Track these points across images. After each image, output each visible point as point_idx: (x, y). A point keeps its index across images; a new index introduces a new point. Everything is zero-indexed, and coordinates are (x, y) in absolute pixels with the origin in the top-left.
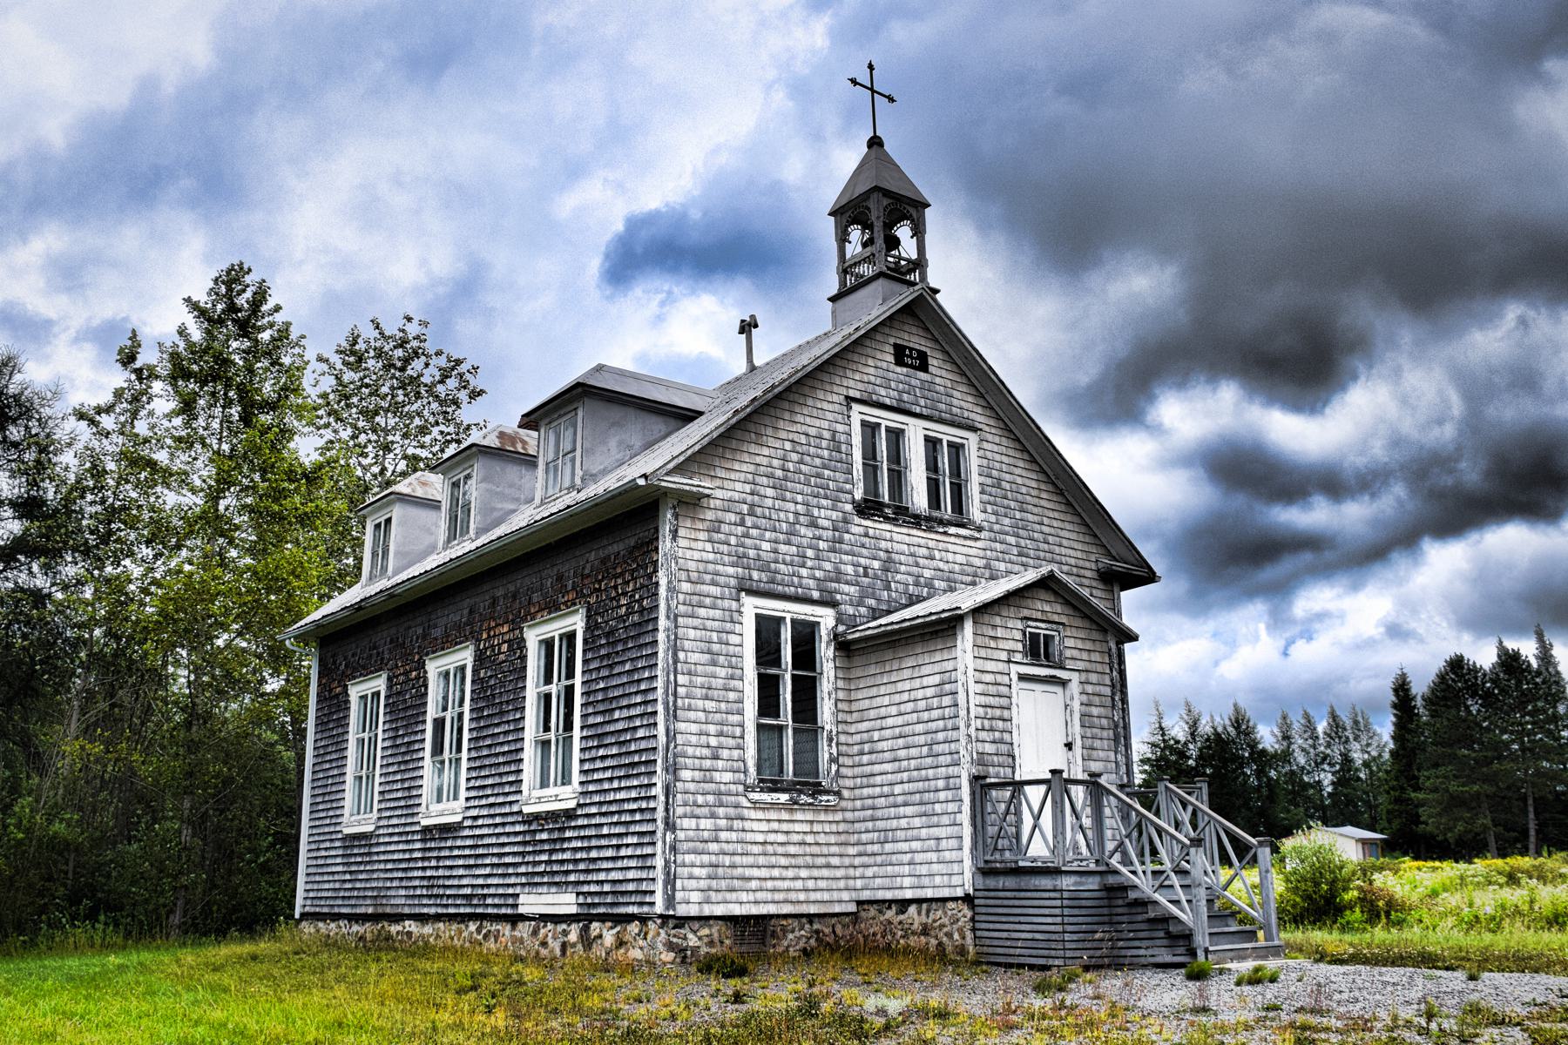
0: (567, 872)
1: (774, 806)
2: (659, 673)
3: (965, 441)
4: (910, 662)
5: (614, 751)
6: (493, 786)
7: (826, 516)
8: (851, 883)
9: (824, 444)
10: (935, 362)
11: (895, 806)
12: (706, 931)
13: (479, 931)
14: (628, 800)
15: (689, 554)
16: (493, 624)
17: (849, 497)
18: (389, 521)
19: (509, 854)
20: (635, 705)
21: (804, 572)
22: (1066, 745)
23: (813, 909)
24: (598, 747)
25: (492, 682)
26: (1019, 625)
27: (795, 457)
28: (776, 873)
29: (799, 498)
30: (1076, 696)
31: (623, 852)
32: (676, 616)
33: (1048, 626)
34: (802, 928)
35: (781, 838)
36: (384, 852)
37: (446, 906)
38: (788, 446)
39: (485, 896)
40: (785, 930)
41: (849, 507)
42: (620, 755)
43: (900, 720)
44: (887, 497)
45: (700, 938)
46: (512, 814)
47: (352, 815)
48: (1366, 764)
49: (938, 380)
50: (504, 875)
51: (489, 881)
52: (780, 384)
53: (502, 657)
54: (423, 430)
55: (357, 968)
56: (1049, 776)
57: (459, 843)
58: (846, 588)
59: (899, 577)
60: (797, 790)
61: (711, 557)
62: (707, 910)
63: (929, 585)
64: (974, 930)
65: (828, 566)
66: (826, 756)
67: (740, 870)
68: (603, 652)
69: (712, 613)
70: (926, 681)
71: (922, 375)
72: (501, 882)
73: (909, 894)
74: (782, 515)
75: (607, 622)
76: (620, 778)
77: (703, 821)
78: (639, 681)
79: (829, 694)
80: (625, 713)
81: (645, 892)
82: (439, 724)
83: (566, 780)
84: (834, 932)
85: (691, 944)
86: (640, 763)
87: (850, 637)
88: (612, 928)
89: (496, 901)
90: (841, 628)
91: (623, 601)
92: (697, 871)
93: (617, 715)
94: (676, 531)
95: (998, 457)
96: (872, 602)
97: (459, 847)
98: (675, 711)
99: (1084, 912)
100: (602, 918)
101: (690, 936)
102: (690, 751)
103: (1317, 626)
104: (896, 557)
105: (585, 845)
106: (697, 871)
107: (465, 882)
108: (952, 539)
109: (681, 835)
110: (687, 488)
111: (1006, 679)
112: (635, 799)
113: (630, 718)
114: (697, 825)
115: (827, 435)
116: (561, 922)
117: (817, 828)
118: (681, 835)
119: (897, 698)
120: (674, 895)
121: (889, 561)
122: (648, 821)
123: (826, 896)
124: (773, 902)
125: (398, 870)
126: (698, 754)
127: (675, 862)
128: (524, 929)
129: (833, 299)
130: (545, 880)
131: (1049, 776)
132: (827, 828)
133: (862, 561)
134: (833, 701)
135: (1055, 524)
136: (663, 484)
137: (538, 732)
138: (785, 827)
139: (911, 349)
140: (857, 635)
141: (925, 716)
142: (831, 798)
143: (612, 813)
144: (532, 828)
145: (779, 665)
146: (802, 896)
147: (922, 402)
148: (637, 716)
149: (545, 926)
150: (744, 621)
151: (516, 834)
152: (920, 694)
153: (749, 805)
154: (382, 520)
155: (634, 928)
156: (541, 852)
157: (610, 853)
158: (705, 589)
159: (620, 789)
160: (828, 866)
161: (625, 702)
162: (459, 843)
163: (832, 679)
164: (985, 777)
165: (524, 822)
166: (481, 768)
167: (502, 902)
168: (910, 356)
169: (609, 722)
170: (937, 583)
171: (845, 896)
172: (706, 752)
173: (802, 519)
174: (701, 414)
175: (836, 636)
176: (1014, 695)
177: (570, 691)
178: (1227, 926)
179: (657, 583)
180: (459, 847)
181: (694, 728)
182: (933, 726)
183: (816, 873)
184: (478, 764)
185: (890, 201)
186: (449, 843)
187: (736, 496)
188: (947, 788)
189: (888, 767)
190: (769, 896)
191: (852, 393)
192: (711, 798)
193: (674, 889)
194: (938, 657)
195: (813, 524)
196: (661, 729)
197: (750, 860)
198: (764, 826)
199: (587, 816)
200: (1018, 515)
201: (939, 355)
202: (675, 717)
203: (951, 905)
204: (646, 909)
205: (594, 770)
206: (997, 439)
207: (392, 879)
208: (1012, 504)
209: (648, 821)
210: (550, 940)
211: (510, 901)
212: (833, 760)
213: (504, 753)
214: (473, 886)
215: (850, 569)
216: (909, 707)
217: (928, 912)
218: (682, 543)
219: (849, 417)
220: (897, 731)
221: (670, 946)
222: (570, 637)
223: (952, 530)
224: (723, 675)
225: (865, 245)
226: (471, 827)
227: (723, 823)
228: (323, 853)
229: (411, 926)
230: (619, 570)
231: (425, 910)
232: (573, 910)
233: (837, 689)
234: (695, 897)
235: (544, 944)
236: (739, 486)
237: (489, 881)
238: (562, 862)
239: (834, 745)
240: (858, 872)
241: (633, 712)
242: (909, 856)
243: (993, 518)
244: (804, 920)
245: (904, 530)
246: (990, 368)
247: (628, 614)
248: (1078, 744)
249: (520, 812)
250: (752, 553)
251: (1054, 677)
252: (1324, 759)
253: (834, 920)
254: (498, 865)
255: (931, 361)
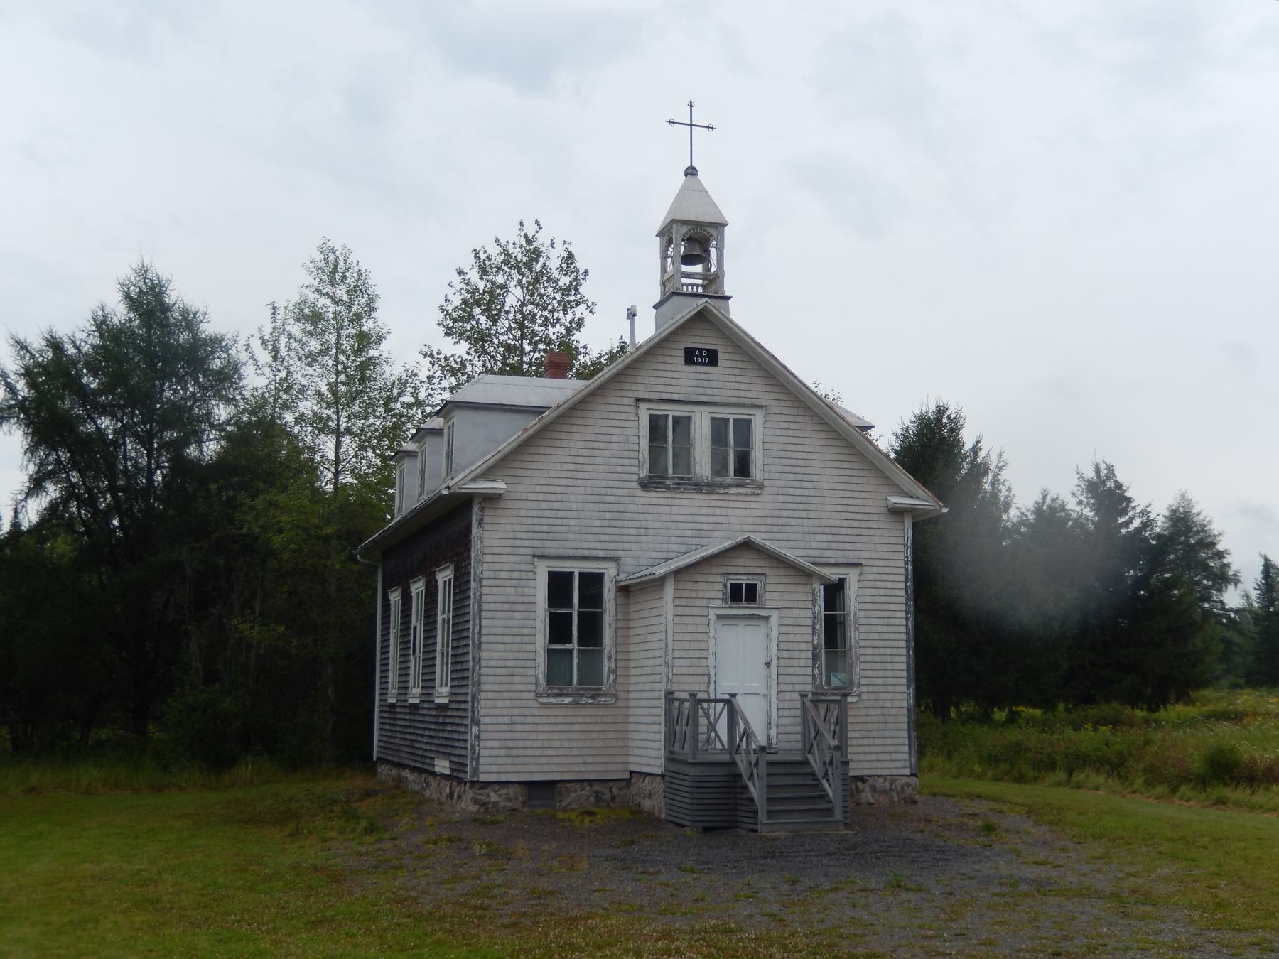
10: (726, 356)
22: (766, 664)
23: (593, 777)
26: (721, 579)
33: (749, 577)
34: (584, 789)
40: (568, 791)
44: (670, 471)
45: (500, 796)
52: (565, 403)
79: (610, 624)
84: (611, 792)
85: (492, 799)
94: (482, 519)
99: (711, 790)
101: (492, 794)
108: (733, 498)
111: (705, 620)
118: (483, 728)
127: (479, 745)
129: (656, 307)
134: (613, 629)
139: (701, 350)
142: (609, 699)
167: (419, 759)
168: (701, 356)
178: (816, 804)
185: (689, 227)
201: (730, 349)
212: (610, 672)
218: (487, 527)
219: (637, 414)
221: (475, 801)
223: (733, 490)
232: (448, 772)
233: (616, 620)
239: (612, 660)
244: (586, 784)
246: (772, 356)
248: (774, 662)
253: (611, 784)
255: (720, 356)
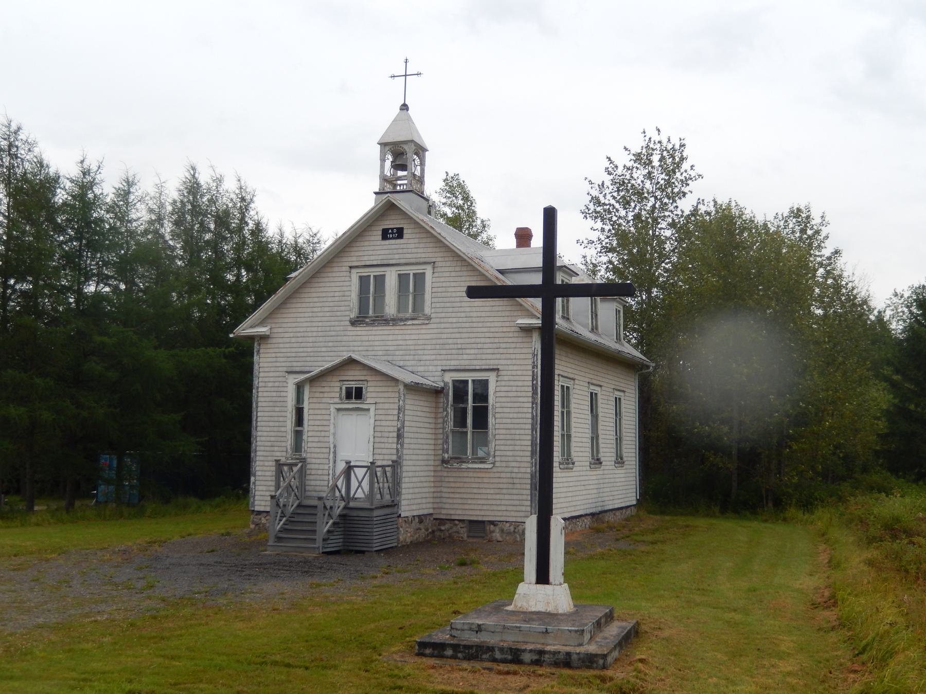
3: (385, 273)
33: (356, 383)
45: (267, 520)
55: (507, 557)
56: (370, 464)
101: (263, 519)
136: (242, 334)
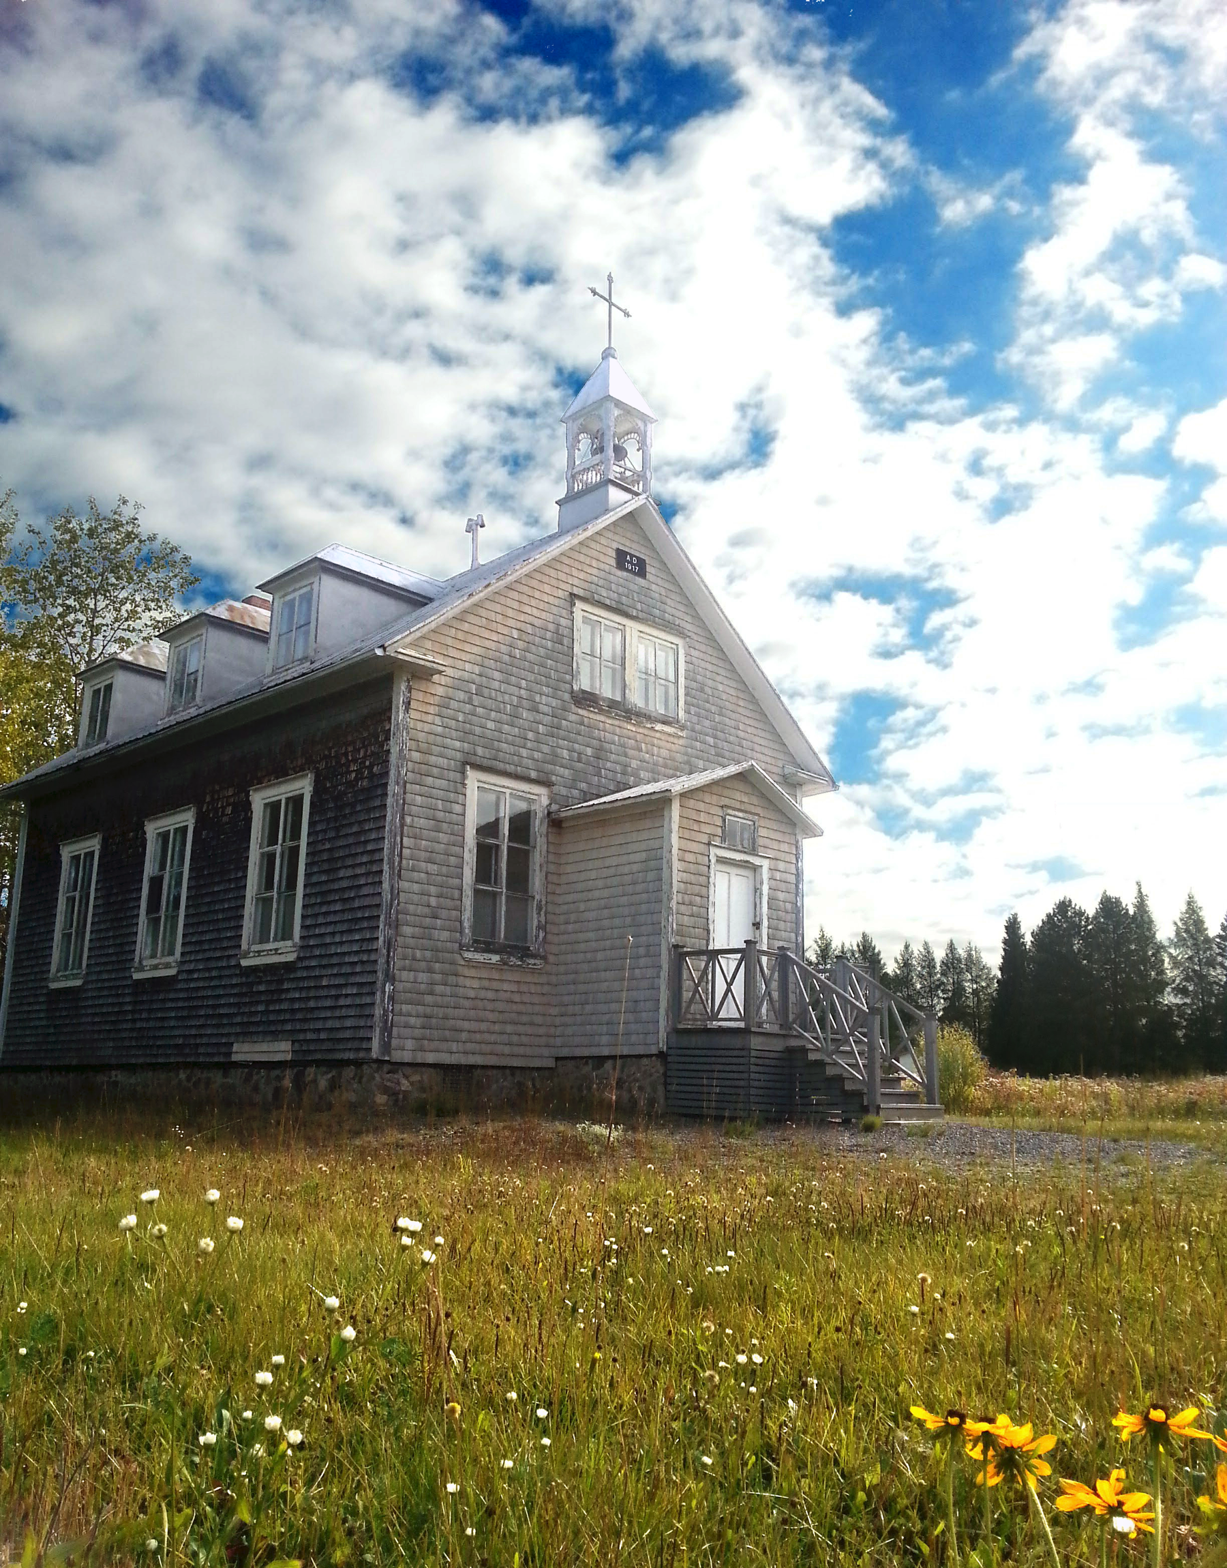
0: (285, 1021)
1: (485, 965)
2: (386, 835)
4: (621, 839)
5: (338, 907)
6: (211, 941)
7: (546, 702)
8: (552, 1041)
9: (549, 635)
11: (597, 971)
12: (416, 1078)
13: (189, 1079)
14: (349, 953)
15: (419, 726)
16: (217, 787)
17: (568, 686)
18: (109, 688)
19: (224, 1005)
20: (361, 864)
21: (524, 752)
23: (516, 1063)
24: (321, 904)
25: (214, 843)
27: (520, 644)
28: (484, 1026)
29: (523, 683)
30: (766, 881)
31: (342, 1002)
32: (405, 782)
35: (490, 995)
36: (91, 1006)
37: (156, 1056)
38: (515, 634)
39: (197, 1045)
41: (567, 697)
42: (343, 911)
43: (606, 893)
45: (412, 1084)
46: (229, 967)
47: (58, 971)
48: (975, 992)
49: (654, 587)
50: (217, 1026)
51: (203, 1032)
53: (225, 819)
54: (133, 615)
56: (744, 946)
57: (172, 996)
58: (561, 770)
59: (609, 765)
60: (508, 953)
61: (440, 729)
62: (420, 1058)
63: (636, 776)
64: (666, 1084)
65: (546, 749)
66: (535, 923)
67: (452, 1022)
68: (330, 814)
69: (438, 782)
70: (632, 858)
71: (640, 580)
72: (215, 1032)
73: (606, 1052)
74: (507, 697)
75: (335, 787)
76: (342, 933)
77: (421, 974)
78: (366, 842)
79: (541, 866)
80: (349, 872)
81: (362, 1039)
82: (156, 882)
83: (286, 934)
86: (363, 918)
87: (563, 815)
88: (326, 1073)
89: (210, 1050)
90: (554, 807)
91: (353, 767)
92: (412, 1020)
93: (342, 874)
95: (703, 664)
96: (583, 786)
97: (172, 1000)
98: (400, 871)
100: (319, 1063)
102: (411, 908)
103: (984, 819)
104: (607, 746)
105: (304, 995)
106: (412, 1020)
107: (176, 1032)
108: (658, 735)
109: (399, 986)
110: (422, 662)
112: (357, 953)
113: (356, 876)
114: (415, 978)
115: (551, 627)
116: (274, 1068)
117: (524, 988)
118: (399, 986)
119: (606, 872)
120: (389, 1042)
121: (601, 749)
122: (369, 972)
123: (529, 1051)
124: (481, 1054)
125: (106, 1022)
126: (419, 912)
128: (235, 1077)
130: (260, 1029)
131: (744, 946)
132: (533, 989)
133: (576, 746)
135: (750, 730)
136: (400, 657)
137: (259, 889)
138: (495, 985)
139: (632, 556)
140: (570, 813)
141: (630, 889)
143: (332, 965)
144: (250, 980)
145: (497, 837)
146: (507, 1050)
147: (639, 606)
148: (362, 875)
149: (258, 1073)
150: (468, 792)
151: (233, 986)
152: (626, 869)
153: (463, 963)
154: (102, 686)
155: (349, 1072)
156: (258, 1003)
157: (328, 1003)
158: (433, 759)
159: (342, 943)
160: (532, 1024)
161: (349, 862)
162: (172, 996)
163: (544, 853)
164: (683, 947)
165: (241, 975)
166: (199, 924)
169: (333, 881)
170: (642, 774)
171: (546, 1052)
172: (426, 910)
173: (525, 703)
174: (431, 600)
175: (549, 813)
176: (712, 875)
177: (294, 852)
179: (388, 751)
180: (172, 1000)
181: (416, 887)
182: (636, 898)
183: (521, 1029)
184: (195, 920)
186: (161, 997)
187: (466, 676)
188: (647, 955)
189: (591, 935)
190: (476, 1047)
191: (576, 591)
192: (428, 954)
193: (390, 1036)
194: (645, 835)
195: (535, 709)
196: (386, 886)
197: (461, 1012)
198: (476, 984)
199: (307, 968)
200: (717, 718)
201: (657, 564)
202: (399, 876)
203: (645, 1061)
204: (362, 1055)
205: (316, 926)
206: (703, 648)
207: (99, 1032)
208: (713, 709)
209: (369, 972)
210: (262, 1086)
211: (223, 1050)
213: (223, 910)
214: (185, 1036)
215: (565, 753)
216: (615, 881)
217: (623, 1067)
218: (413, 714)
219: (572, 612)
220: (603, 902)
222: (297, 801)
224: (445, 841)
225: (594, 453)
226: (186, 980)
227: (438, 977)
228: (26, 1008)
229: (119, 1076)
230: (350, 738)
231: (133, 1061)
232: (289, 1057)
234: (409, 1044)
235: (256, 1089)
236: (468, 667)
237: (203, 1032)
238: (280, 1011)
240: (559, 1031)
241: (359, 871)
242: (608, 1016)
243: (695, 719)
245: (617, 723)
247: (356, 779)
249: (239, 965)
250: (478, 730)
251: (747, 862)
252: (938, 987)
254: (212, 1016)
255: (648, 568)
